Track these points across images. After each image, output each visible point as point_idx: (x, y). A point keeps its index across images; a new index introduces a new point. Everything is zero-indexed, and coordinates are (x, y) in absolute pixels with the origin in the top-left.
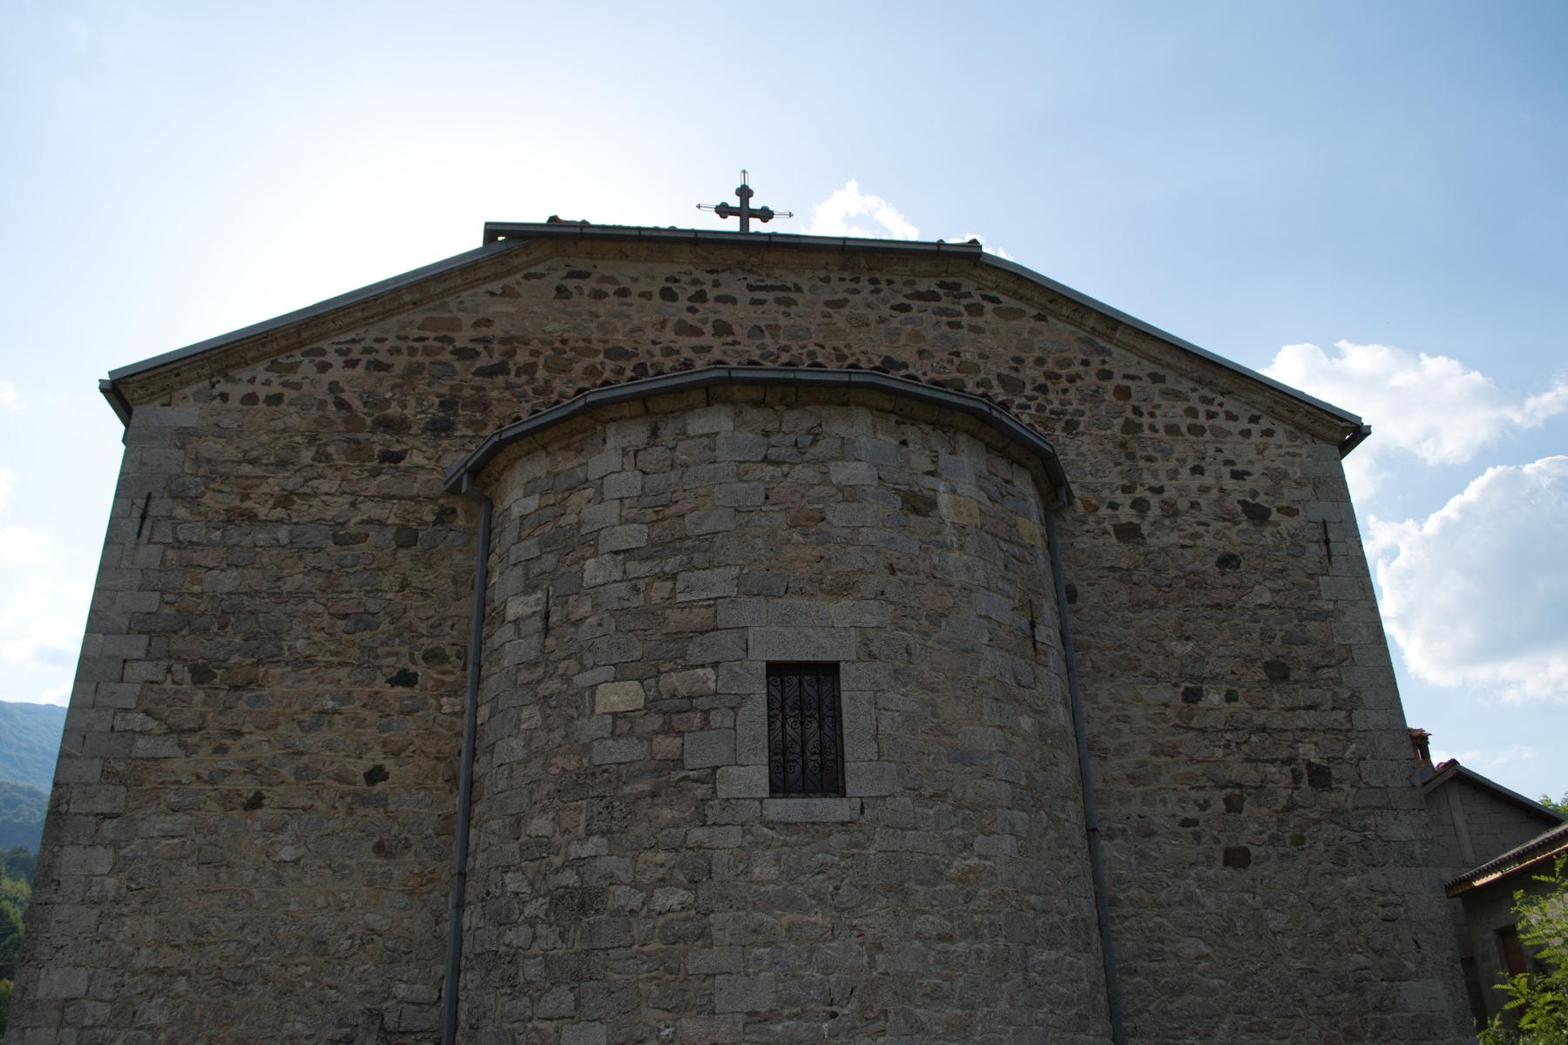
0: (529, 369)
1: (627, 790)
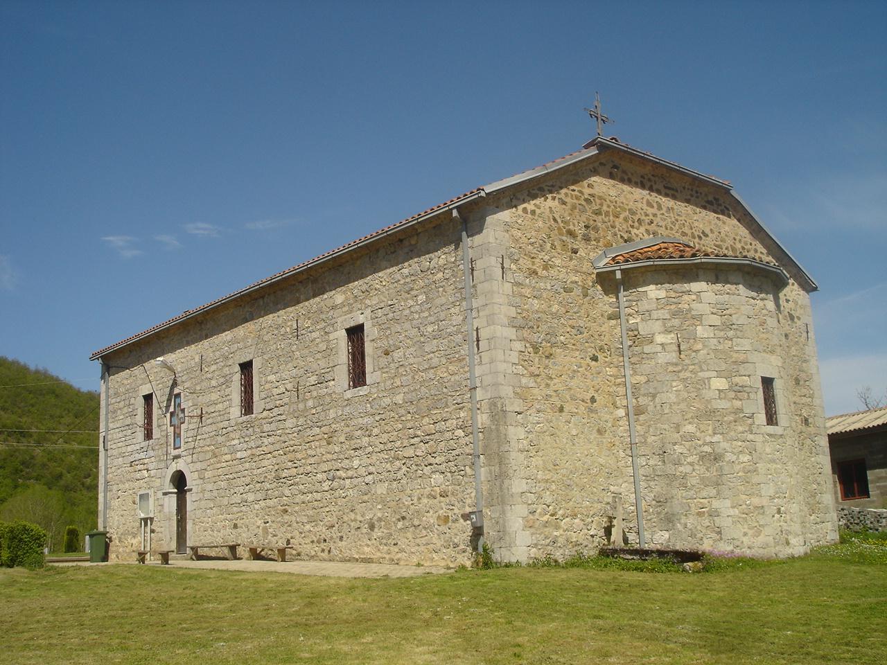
0: (607, 214)
1: (726, 419)
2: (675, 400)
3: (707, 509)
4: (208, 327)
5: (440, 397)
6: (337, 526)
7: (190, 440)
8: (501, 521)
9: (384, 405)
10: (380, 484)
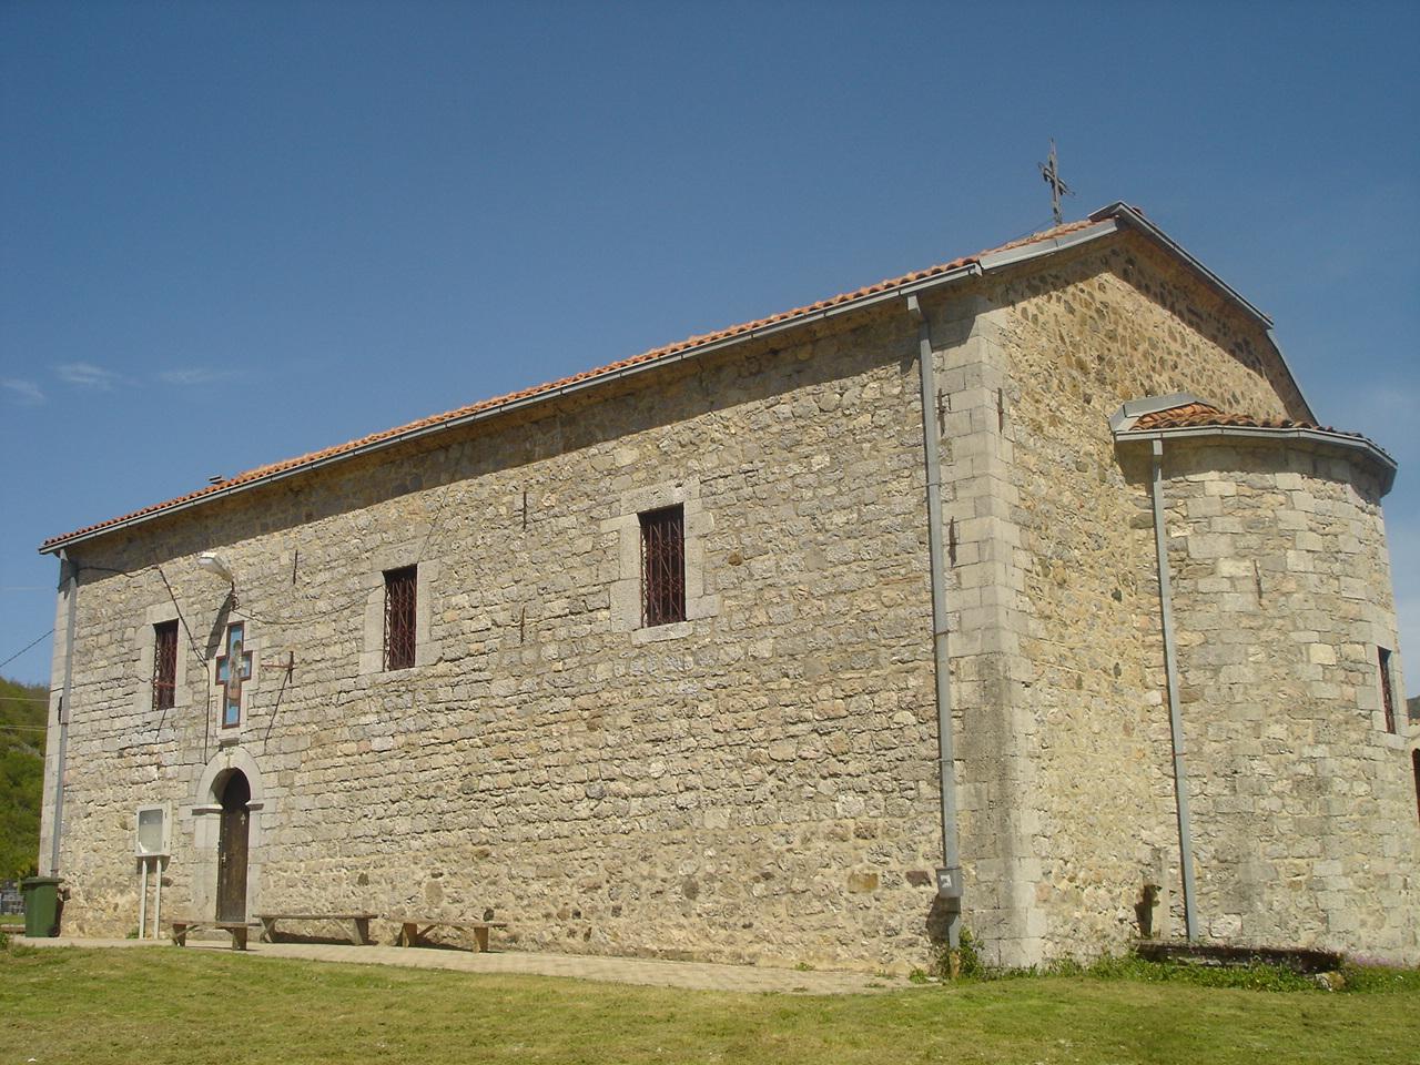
1: (1333, 717)
2: (1253, 680)
3: (1305, 877)
4: (313, 500)
5: (860, 647)
6: (606, 887)
7: (262, 711)
8: (1001, 888)
9: (727, 660)
10: (713, 809)
